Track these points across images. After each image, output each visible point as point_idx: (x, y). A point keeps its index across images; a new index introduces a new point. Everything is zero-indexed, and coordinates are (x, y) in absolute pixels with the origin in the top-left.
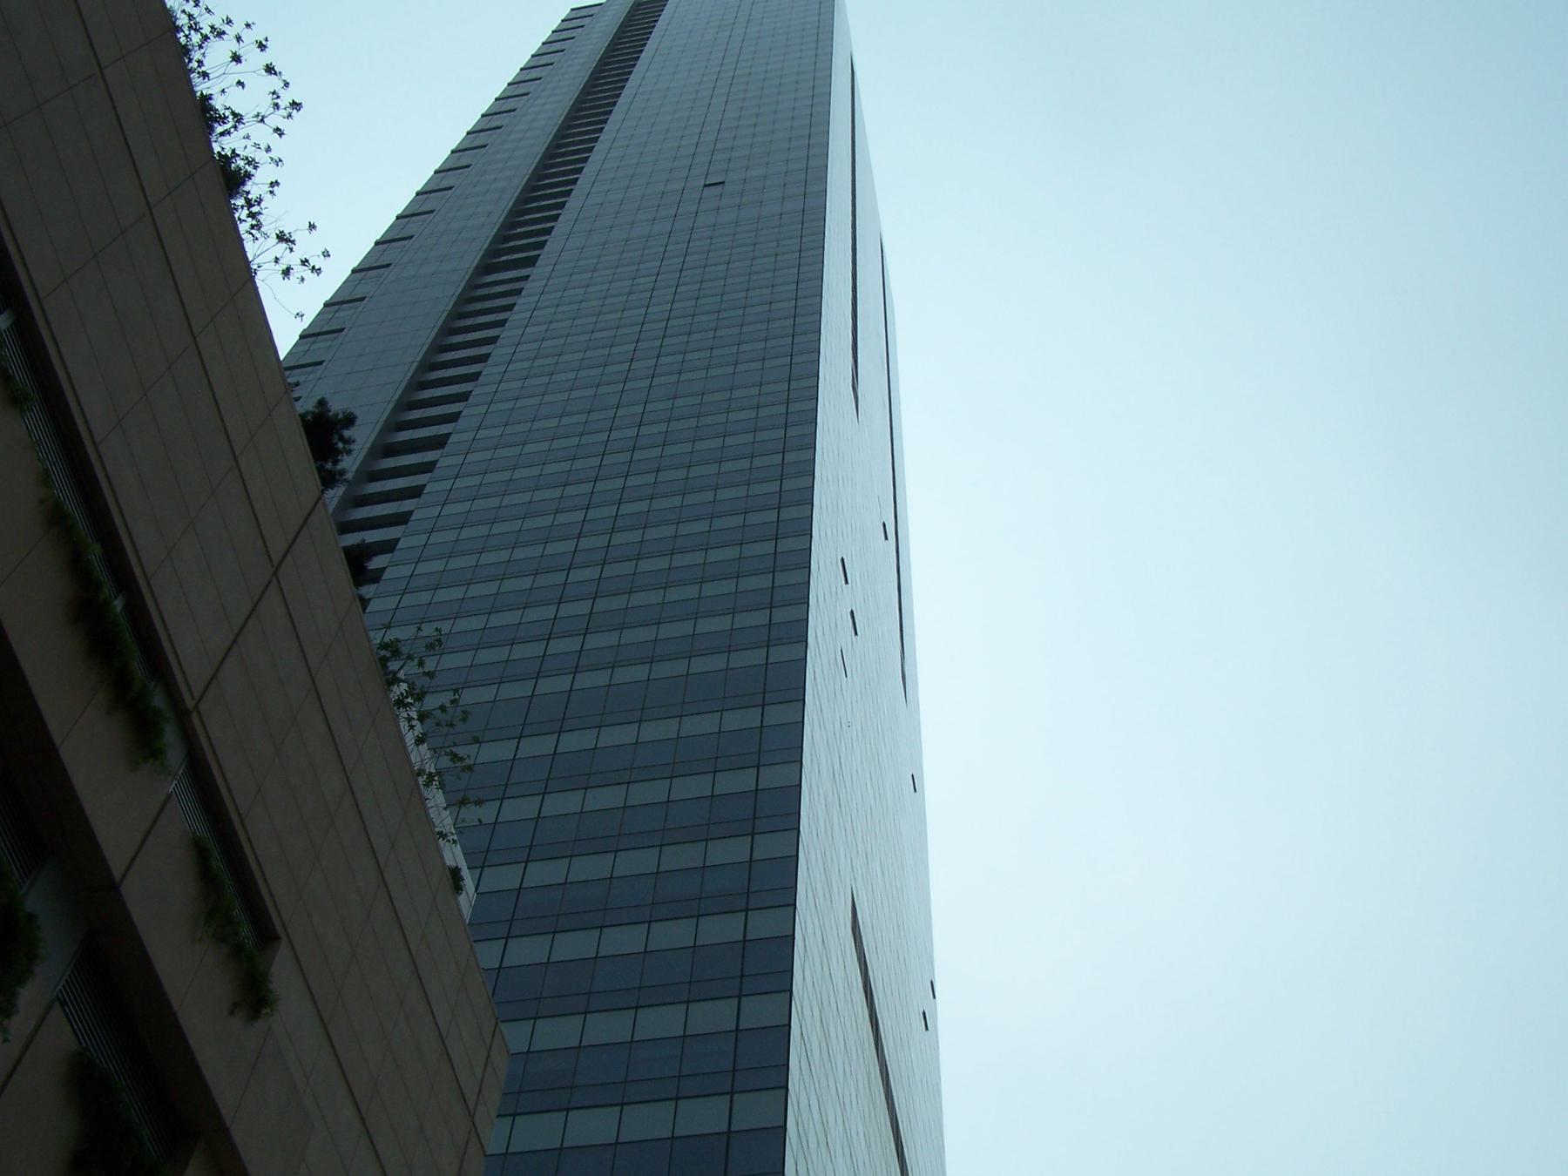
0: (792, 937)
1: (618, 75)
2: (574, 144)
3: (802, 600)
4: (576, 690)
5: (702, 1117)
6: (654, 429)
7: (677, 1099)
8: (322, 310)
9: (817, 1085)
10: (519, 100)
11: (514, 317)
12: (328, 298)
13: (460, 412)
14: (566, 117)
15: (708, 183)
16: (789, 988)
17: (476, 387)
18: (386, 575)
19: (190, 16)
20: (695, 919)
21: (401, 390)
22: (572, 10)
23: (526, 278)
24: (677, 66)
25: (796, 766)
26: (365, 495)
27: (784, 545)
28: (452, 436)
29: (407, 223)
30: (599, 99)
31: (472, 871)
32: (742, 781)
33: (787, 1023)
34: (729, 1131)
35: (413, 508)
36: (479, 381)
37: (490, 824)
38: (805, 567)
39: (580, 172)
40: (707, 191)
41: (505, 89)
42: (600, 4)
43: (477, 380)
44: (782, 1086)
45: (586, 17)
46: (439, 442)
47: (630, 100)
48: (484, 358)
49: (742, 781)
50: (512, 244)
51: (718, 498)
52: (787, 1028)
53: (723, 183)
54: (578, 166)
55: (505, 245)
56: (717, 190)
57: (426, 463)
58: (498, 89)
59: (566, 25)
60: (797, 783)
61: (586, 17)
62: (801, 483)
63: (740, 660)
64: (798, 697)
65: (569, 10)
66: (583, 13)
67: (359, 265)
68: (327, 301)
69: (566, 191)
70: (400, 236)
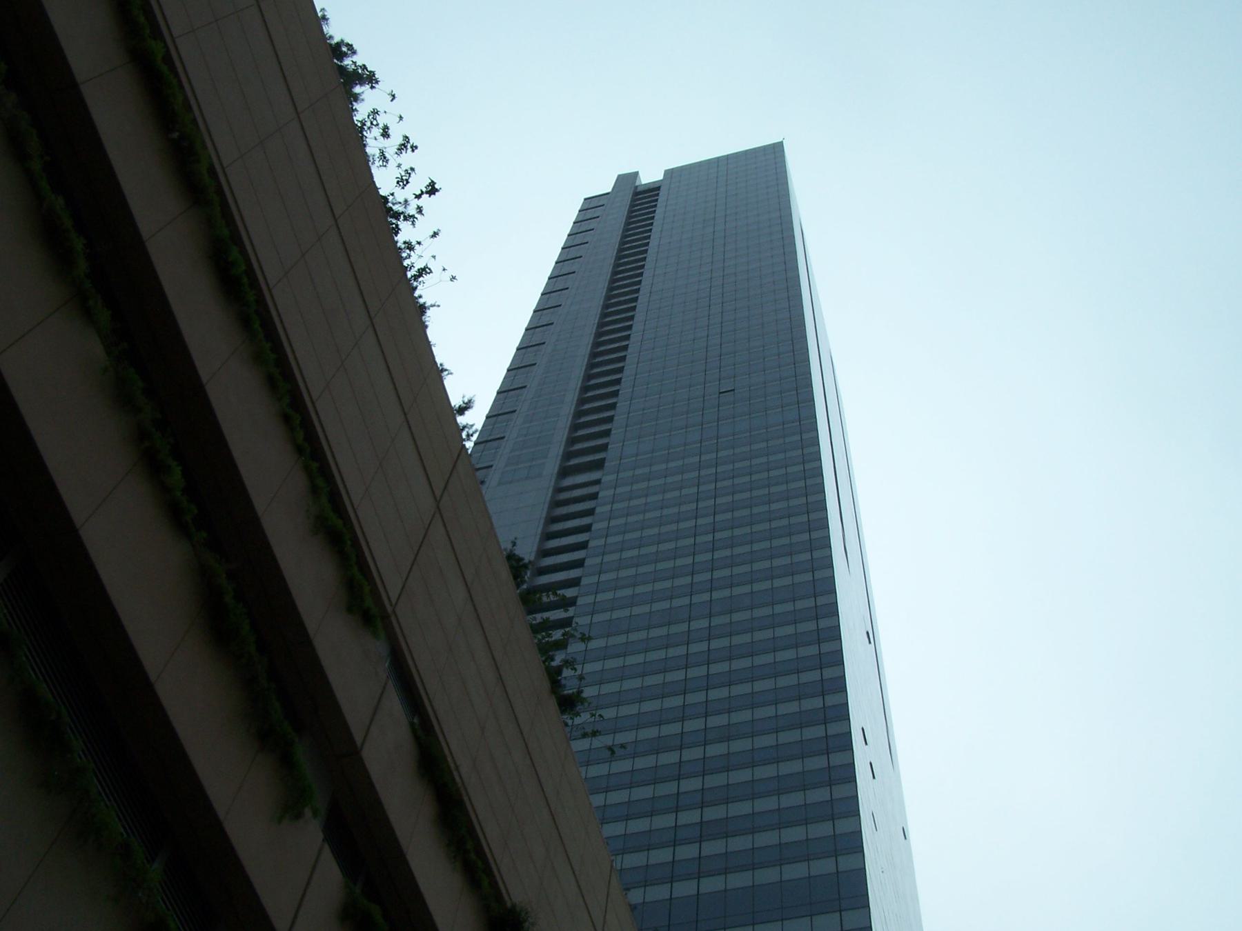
1: (647, 208)
2: (613, 331)
5: (824, 867)
6: (726, 483)
8: (496, 397)
12: (487, 412)
14: (631, 201)
16: (849, 730)
17: (603, 475)
18: (600, 495)
19: (368, 118)
22: (585, 199)
23: (598, 482)
25: (857, 817)
26: (547, 549)
27: (811, 499)
28: (579, 599)
29: (541, 315)
42: (608, 194)
44: (867, 906)
50: (618, 284)
52: (863, 870)
55: (609, 302)
57: (573, 579)
62: (812, 449)
64: (832, 591)
65: (583, 200)
69: (621, 357)
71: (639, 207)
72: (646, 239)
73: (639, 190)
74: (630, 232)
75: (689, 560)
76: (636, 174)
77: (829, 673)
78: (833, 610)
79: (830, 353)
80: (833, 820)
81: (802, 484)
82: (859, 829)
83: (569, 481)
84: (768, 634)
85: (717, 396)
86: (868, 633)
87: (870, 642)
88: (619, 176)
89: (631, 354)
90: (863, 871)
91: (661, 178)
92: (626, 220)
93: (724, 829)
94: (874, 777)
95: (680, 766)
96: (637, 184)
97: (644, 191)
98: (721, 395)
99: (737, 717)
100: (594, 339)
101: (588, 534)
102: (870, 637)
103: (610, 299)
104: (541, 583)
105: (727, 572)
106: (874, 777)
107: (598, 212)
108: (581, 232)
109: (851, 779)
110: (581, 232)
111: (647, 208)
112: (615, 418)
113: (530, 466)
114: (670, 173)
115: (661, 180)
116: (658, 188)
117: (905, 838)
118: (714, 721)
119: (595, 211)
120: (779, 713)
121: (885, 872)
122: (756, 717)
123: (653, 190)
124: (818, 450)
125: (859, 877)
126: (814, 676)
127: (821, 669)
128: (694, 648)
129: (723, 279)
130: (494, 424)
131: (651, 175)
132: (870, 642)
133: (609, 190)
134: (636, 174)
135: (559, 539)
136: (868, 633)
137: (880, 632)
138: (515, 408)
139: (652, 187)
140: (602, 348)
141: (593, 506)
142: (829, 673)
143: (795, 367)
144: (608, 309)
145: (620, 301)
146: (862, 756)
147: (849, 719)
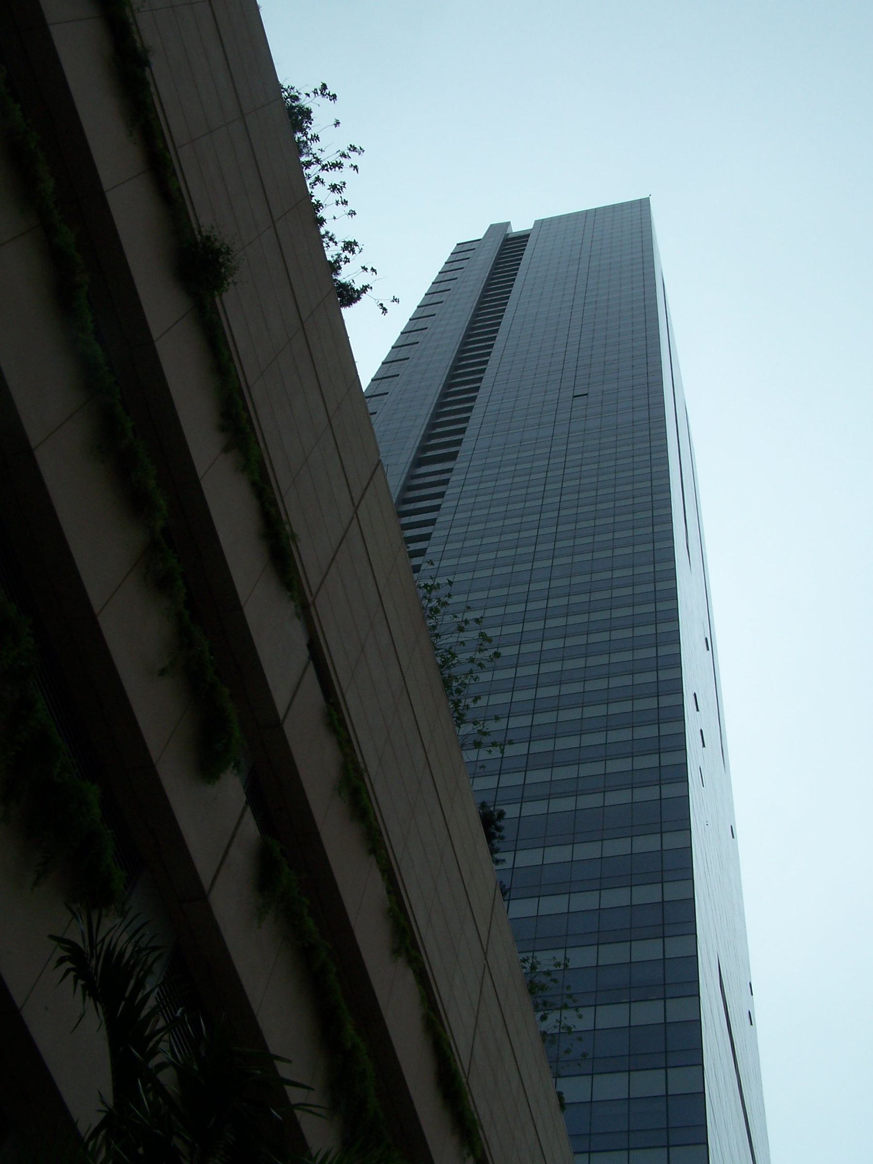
0: (693, 899)
3: (677, 665)
4: (523, 817)
5: (648, 844)
7: (629, 1071)
9: (706, 807)
10: (435, 307)
11: (457, 466)
13: (436, 519)
15: (575, 395)
20: (630, 839)
21: (433, 408)
22: (458, 244)
23: (450, 470)
24: (542, 294)
30: (486, 320)
31: (594, 210)
32: (650, 793)
33: (696, 954)
34: (663, 901)
35: (421, 563)
36: (457, 460)
37: (494, 788)
38: (679, 693)
39: (510, 293)
40: (578, 401)
41: (455, 248)
42: (480, 240)
43: (443, 497)
44: (693, 933)
45: (463, 260)
46: (453, 457)
47: (510, 322)
48: (446, 482)
49: (650, 793)
51: (616, 491)
53: (587, 394)
54: (490, 343)
56: (583, 400)
58: (433, 276)
59: (455, 258)
60: (682, 703)
61: (463, 260)
63: (641, 795)
65: (456, 245)
66: (466, 247)
67: (375, 376)
68: (372, 378)
70: (414, 329)
71: (500, 270)
72: (491, 341)
73: (510, 236)
74: (495, 281)
75: (518, 628)
76: (508, 224)
77: (668, 759)
78: (673, 616)
79: (685, 402)
80: (660, 785)
81: (651, 587)
82: (684, 731)
83: (423, 470)
84: (600, 710)
85: (571, 399)
86: (706, 639)
87: (708, 649)
88: (491, 225)
89: (482, 395)
90: (691, 901)
91: (531, 227)
92: (477, 305)
93: (552, 761)
94: (704, 746)
95: (537, 538)
96: (508, 232)
97: (514, 238)
98: (574, 398)
99: (563, 743)
100: (443, 389)
101: (446, 486)
102: (709, 644)
103: (438, 418)
104: (415, 484)
105: (561, 622)
106: (704, 746)
107: (469, 254)
108: (452, 271)
109: (681, 747)
110: (452, 271)
111: (501, 288)
112: (489, 362)
113: (387, 456)
114: (539, 224)
115: (531, 229)
116: (529, 235)
117: (733, 837)
118: (535, 776)
119: (472, 245)
120: (611, 661)
121: (709, 824)
122: (586, 716)
123: (523, 238)
124: (667, 469)
125: (683, 802)
126: (651, 761)
127: (657, 671)
128: (519, 696)
129: (583, 313)
130: (389, 367)
131: (518, 227)
132: (708, 649)
133: (481, 237)
134: (508, 224)
135: (408, 517)
136: (706, 639)
137: (708, 563)
138: (398, 373)
139: (522, 234)
140: (433, 442)
141: (466, 426)
142: (668, 759)
143: (648, 387)
144: (434, 429)
145: (507, 261)
146: (693, 722)
147: (686, 749)
